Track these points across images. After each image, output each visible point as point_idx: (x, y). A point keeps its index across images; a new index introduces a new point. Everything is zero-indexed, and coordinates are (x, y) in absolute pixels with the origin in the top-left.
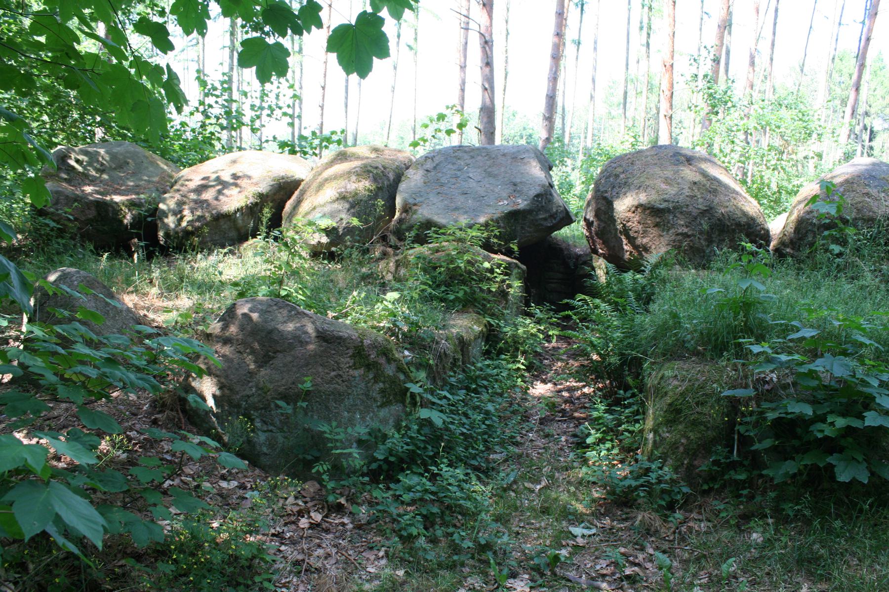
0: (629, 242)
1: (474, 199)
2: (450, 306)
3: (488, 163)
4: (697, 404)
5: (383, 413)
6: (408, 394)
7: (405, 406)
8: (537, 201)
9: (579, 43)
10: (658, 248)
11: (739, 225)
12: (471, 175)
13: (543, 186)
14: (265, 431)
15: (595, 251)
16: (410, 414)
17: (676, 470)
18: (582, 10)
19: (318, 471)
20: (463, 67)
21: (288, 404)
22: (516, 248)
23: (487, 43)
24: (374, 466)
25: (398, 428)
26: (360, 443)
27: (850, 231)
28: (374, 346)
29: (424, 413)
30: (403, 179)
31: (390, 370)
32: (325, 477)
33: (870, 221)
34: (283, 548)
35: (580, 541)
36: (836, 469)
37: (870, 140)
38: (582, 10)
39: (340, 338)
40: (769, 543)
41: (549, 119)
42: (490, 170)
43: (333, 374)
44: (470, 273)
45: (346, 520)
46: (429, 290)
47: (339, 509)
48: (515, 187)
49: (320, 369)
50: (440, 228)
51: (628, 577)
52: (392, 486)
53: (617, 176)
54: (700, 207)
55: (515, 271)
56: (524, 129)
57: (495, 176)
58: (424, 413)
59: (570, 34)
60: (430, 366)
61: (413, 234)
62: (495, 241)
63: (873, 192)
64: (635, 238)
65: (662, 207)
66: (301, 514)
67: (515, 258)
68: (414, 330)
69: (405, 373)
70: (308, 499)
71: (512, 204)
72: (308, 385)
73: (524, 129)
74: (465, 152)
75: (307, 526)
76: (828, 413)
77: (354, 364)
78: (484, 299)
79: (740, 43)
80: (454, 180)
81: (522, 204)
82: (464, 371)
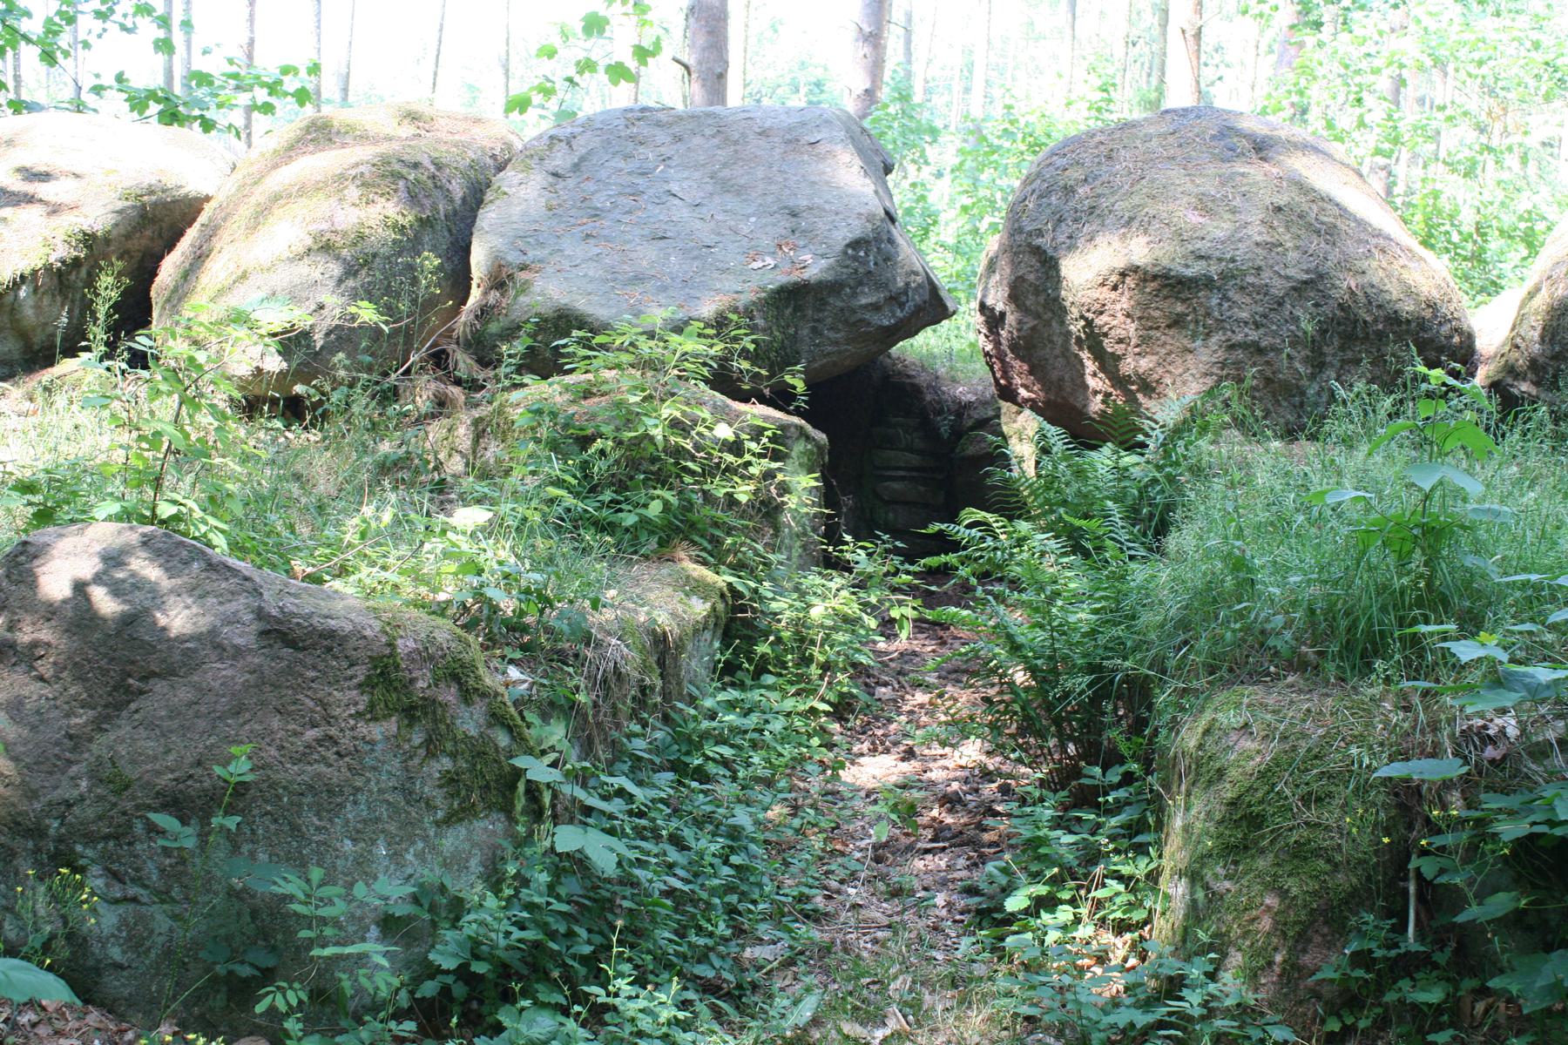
0: (1102, 368)
1: (684, 251)
3: (722, 154)
5: (452, 840)
6: (521, 787)
7: (512, 820)
8: (855, 258)
12: (675, 188)
13: (870, 218)
14: (116, 902)
15: (1008, 393)
19: (272, 1010)
24: (429, 989)
25: (494, 880)
26: (389, 925)
28: (425, 655)
29: (568, 838)
30: (489, 196)
31: (470, 722)
32: (292, 1025)
39: (331, 634)
42: (726, 173)
43: (311, 734)
44: (678, 452)
46: (570, 501)
49: (276, 722)
53: (1069, 191)
54: (1291, 272)
55: (799, 447)
57: (740, 191)
58: (568, 838)
62: (745, 365)
64: (1118, 358)
71: (787, 267)
72: (240, 768)
74: (659, 124)
77: (372, 706)
78: (716, 525)
81: (814, 266)
82: (666, 719)
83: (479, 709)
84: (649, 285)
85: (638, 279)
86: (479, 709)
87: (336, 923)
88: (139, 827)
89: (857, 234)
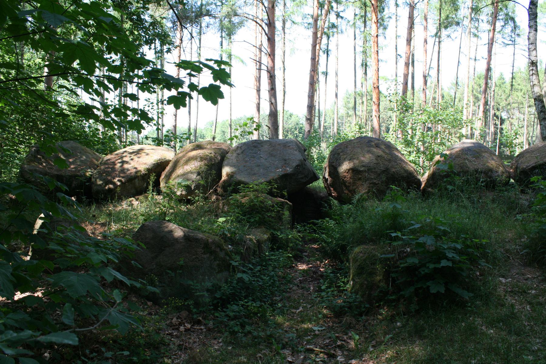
3: (271, 149)
4: (371, 264)
5: (219, 276)
6: (231, 267)
7: (230, 272)
9: (327, 74)
10: (362, 190)
12: (262, 156)
13: (300, 160)
14: (160, 287)
15: (330, 195)
17: (362, 296)
18: (328, 54)
19: (188, 304)
22: (286, 194)
23: (272, 77)
24: (215, 302)
25: (226, 282)
26: (208, 290)
27: (457, 178)
28: (214, 242)
29: (239, 275)
30: (225, 159)
31: (222, 255)
32: (191, 306)
33: (466, 172)
34: (172, 339)
35: (317, 332)
37: (501, 124)
38: (328, 54)
39: (197, 239)
40: (404, 326)
43: (194, 257)
44: (262, 208)
45: (202, 327)
46: (241, 217)
47: (199, 323)
48: (286, 162)
49: (188, 255)
50: (246, 185)
51: (339, 346)
52: (225, 310)
53: (339, 154)
54: (382, 168)
55: (286, 206)
56: (297, 124)
58: (239, 275)
59: (321, 68)
61: (231, 188)
62: (275, 190)
65: (362, 169)
66: (180, 324)
67: (286, 199)
68: (233, 236)
72: (182, 263)
73: (297, 124)
74: (258, 143)
75: (183, 330)
76: (427, 263)
77: (204, 252)
78: (270, 221)
79: (419, 71)
80: (252, 159)
81: (289, 170)
82: (260, 257)
85: (254, 174)
88: (164, 273)
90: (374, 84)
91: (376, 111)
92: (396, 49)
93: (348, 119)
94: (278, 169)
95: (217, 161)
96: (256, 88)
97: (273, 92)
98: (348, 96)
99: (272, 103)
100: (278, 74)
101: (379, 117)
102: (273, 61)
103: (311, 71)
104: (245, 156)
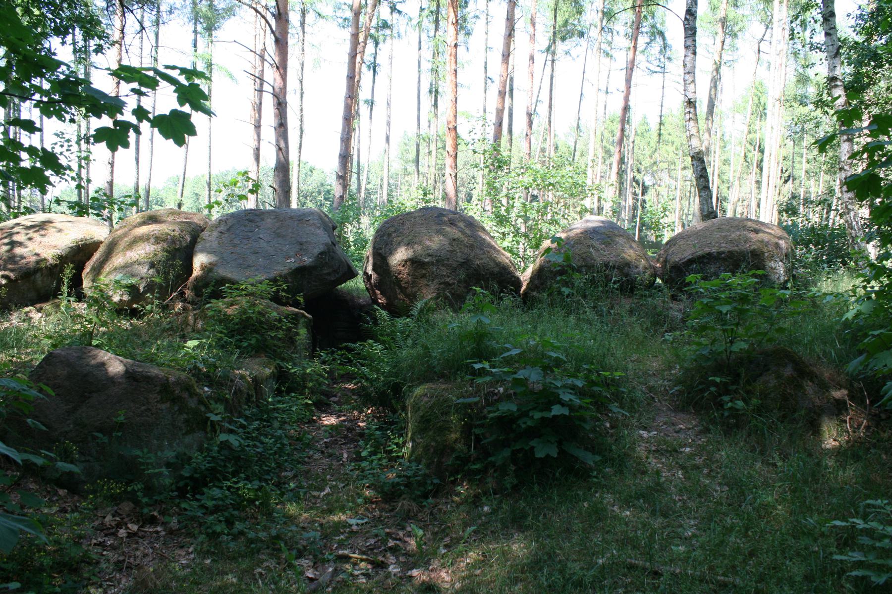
0: (402, 292)
1: (264, 257)
2: (244, 353)
5: (188, 439)
6: (209, 423)
7: (206, 433)
9: (372, 103)
11: (492, 274)
12: (261, 236)
13: (326, 244)
15: (375, 301)
16: (212, 439)
17: (428, 466)
19: (133, 489)
20: (258, 127)
21: (104, 435)
23: (281, 106)
24: (181, 484)
25: (201, 449)
26: (168, 465)
28: (178, 383)
29: (223, 437)
30: (199, 240)
32: (139, 494)
33: (590, 267)
34: (105, 553)
35: (355, 528)
36: (535, 450)
37: (643, 194)
40: (494, 512)
41: (343, 178)
42: (279, 231)
43: (143, 408)
44: (261, 322)
45: (159, 529)
47: (153, 521)
48: (302, 247)
51: (391, 548)
52: (198, 497)
53: (390, 235)
55: (302, 320)
56: (322, 185)
57: (283, 237)
58: (223, 437)
59: (364, 94)
60: (227, 400)
61: (209, 290)
62: (284, 294)
63: (596, 244)
64: (406, 288)
65: (427, 260)
66: (119, 526)
67: (302, 309)
68: (212, 371)
69: (205, 405)
70: (124, 516)
72: (121, 419)
73: (322, 185)
74: (256, 215)
75: (125, 535)
77: (162, 399)
79: (520, 104)
80: (245, 241)
81: (307, 260)
82: (258, 406)
83: (195, 399)
84: (252, 269)
85: (249, 267)
86: (195, 399)
87: (151, 464)
88: (90, 438)
89: (322, 250)
90: (449, 123)
91: (451, 167)
92: (486, 68)
93: (407, 178)
94: (289, 258)
95: (184, 244)
96: (253, 122)
97: (282, 129)
98: (406, 141)
99: (280, 149)
100: (292, 100)
101: (456, 176)
102: (284, 77)
103: (346, 98)
104: (233, 236)
